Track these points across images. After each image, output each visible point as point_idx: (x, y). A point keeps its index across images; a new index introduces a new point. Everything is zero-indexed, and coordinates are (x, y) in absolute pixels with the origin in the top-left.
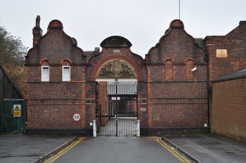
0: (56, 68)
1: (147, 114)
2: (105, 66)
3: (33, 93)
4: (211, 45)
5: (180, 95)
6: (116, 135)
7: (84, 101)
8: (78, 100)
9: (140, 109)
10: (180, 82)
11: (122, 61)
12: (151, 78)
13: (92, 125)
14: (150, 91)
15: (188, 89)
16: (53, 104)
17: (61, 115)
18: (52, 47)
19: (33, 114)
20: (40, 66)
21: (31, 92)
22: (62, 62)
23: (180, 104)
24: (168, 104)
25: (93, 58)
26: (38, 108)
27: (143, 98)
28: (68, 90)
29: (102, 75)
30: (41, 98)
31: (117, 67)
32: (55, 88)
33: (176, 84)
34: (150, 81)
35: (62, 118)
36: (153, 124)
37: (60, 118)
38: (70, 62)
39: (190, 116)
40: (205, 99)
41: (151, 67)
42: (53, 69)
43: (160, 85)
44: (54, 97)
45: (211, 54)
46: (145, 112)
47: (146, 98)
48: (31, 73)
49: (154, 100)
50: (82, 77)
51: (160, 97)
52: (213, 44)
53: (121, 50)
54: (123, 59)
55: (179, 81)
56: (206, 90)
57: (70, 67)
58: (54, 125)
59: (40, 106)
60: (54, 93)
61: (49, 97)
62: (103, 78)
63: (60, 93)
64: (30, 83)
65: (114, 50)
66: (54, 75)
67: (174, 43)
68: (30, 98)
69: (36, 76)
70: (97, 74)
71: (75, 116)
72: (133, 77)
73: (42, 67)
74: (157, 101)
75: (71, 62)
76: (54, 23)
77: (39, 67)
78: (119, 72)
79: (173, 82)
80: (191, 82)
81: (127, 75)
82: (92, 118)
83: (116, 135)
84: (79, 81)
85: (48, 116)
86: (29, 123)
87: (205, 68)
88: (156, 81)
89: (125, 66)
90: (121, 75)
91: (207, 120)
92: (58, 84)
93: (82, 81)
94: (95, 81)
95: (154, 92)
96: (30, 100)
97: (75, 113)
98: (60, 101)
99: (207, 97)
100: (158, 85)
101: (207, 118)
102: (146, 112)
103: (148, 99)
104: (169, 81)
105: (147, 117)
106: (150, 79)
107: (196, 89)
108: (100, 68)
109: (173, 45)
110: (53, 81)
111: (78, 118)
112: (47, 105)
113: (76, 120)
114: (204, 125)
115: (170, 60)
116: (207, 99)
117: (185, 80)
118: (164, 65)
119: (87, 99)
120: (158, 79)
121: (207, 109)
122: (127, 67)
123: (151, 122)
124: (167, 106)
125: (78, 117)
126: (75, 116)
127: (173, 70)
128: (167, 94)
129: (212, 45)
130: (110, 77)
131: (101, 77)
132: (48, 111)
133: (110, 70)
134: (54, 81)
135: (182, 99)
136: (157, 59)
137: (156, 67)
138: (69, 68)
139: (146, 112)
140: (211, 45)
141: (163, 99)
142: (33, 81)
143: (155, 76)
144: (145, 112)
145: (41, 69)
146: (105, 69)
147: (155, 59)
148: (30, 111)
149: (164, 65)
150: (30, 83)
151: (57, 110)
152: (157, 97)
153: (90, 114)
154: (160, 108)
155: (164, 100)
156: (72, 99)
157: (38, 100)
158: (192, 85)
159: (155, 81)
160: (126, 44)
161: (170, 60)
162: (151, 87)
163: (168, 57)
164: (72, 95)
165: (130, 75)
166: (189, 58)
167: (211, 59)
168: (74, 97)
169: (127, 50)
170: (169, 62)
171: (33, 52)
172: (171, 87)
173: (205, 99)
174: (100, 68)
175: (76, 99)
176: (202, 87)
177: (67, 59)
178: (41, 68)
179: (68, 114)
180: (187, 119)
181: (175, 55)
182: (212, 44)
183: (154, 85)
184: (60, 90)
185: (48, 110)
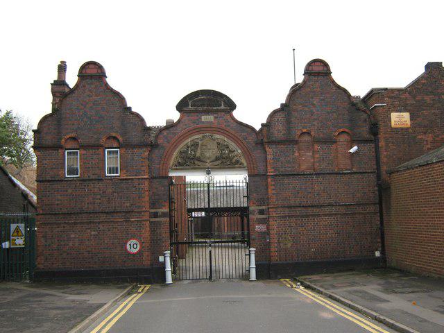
11: (218, 136)
22: (103, 141)
23: (331, 215)
24: (307, 216)
30: (65, 211)
34: (272, 174)
40: (375, 204)
44: (88, 208)
48: (44, 162)
50: (143, 169)
59: (62, 225)
65: (203, 117)
70: (171, 163)
71: (130, 245)
72: (240, 167)
78: (214, 158)
79: (316, 174)
84: (136, 175)
88: (284, 173)
90: (218, 162)
91: (380, 245)
92: (96, 182)
97: (131, 239)
99: (377, 201)
100: (286, 180)
101: (379, 240)
102: (267, 233)
105: (269, 242)
106: (273, 170)
110: (86, 177)
112: (75, 223)
115: (308, 133)
116: (378, 205)
119: (152, 211)
126: (130, 245)
136: (283, 132)
139: (267, 233)
142: (48, 178)
146: (184, 152)
164: (124, 203)
169: (228, 116)
177: (114, 135)
184: (100, 194)
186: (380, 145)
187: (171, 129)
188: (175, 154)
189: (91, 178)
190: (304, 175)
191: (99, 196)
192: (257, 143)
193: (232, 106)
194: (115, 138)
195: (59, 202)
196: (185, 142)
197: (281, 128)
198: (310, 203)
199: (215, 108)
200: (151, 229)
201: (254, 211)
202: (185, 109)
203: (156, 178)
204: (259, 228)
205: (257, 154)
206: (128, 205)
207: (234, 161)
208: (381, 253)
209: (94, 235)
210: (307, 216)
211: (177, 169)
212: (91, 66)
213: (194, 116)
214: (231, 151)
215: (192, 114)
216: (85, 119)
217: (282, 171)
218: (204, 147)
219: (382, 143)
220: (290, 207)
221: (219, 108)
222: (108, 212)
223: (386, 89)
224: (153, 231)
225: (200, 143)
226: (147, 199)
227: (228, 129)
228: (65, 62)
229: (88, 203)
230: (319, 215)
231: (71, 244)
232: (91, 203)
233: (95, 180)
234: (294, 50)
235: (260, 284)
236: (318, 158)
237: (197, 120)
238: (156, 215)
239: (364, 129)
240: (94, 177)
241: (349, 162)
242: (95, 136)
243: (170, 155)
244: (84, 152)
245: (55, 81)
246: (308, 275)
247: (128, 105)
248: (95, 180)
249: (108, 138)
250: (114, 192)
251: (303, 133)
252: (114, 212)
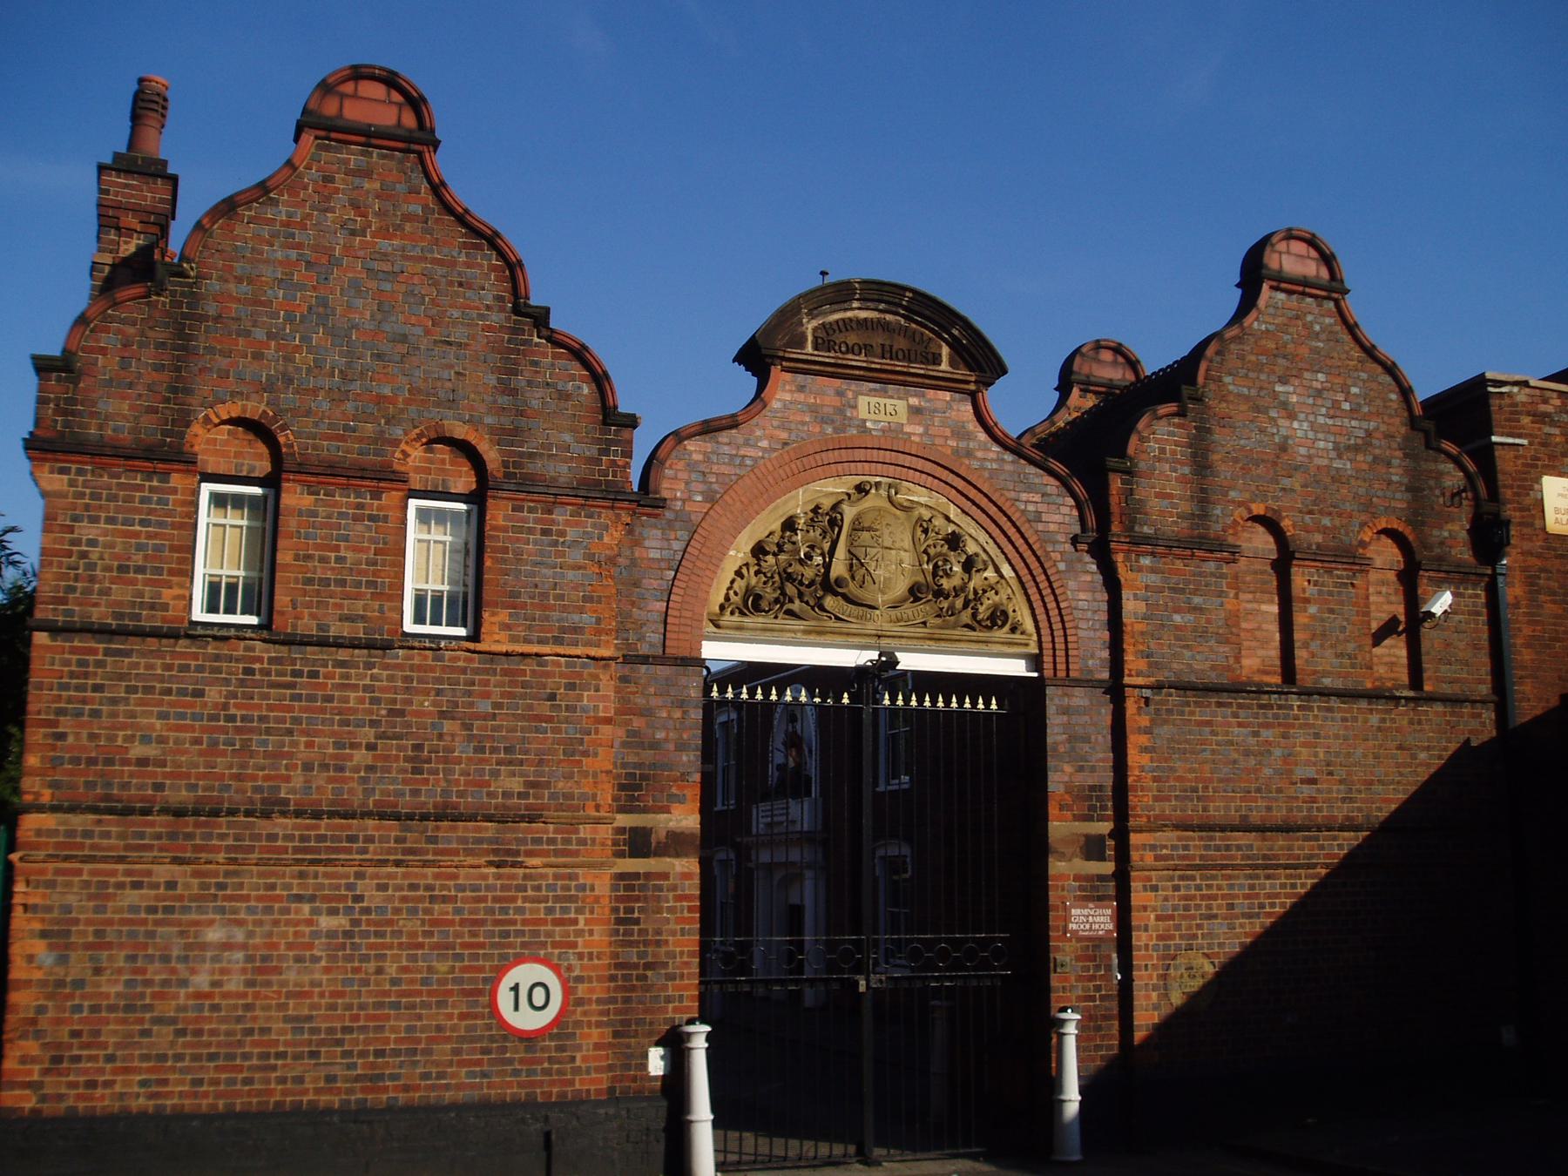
4: (1510, 440)
5: (1344, 800)
9: (1066, 919)
11: (921, 496)
17: (380, 971)
18: (324, 303)
19: (79, 965)
25: (691, 445)
26: (132, 897)
29: (752, 603)
30: (180, 795)
42: (314, 514)
48: (86, 531)
51: (1217, 810)
52: (1520, 436)
53: (914, 401)
60: (309, 745)
63: (371, 747)
65: (863, 401)
68: (54, 785)
69: (140, 570)
71: (516, 988)
75: (490, 466)
76: (355, 96)
77: (176, 480)
82: (669, 1000)
84: (558, 641)
85: (234, 984)
93: (588, 644)
94: (694, 654)
96: (54, 809)
97: (520, 960)
111: (539, 1001)
113: (527, 1020)
119: (623, 820)
125: (539, 996)
129: (1517, 441)
131: (749, 621)
140: (1510, 440)
142: (99, 614)
144: (1100, 939)
148: (44, 934)
151: (340, 922)
152: (1192, 811)
153: (648, 966)
164: (495, 774)
168: (506, 795)
177: (460, 431)
179: (442, 967)
184: (373, 723)
185: (240, 923)
187: (724, 437)
188: (738, 553)
191: (367, 734)
194: (466, 450)
196: (968, 526)
198: (1279, 814)
200: (615, 910)
202: (794, 354)
206: (516, 785)
209: (331, 934)
221: (932, 370)
229: (308, 767)
232: (325, 767)
233: (354, 644)
238: (638, 843)
246: (1050, 1053)
247: (535, 300)
248: (354, 644)
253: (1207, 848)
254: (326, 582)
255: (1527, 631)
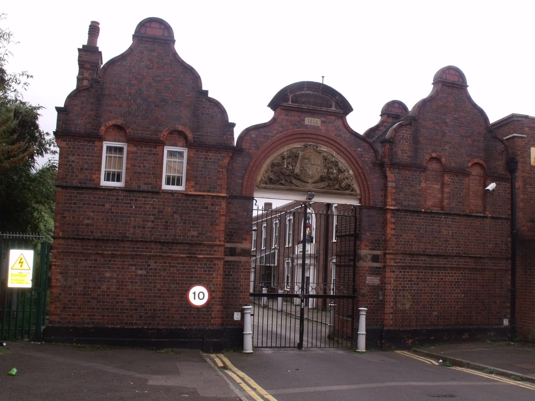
0: (146, 149)
1: (380, 293)
2: (279, 158)
3: (73, 217)
4: (520, 135)
5: (457, 247)
6: (300, 346)
7: (222, 249)
8: (204, 245)
10: (459, 215)
11: (324, 149)
12: (395, 200)
13: (239, 319)
14: (393, 232)
15: (475, 234)
16: (131, 255)
20: (101, 139)
21: (66, 214)
22: (163, 135)
23: (458, 269)
24: (431, 268)
26: (85, 263)
27: (374, 250)
28: (176, 216)
29: (271, 181)
30: (98, 235)
31: (313, 163)
32: (141, 207)
33: (449, 220)
34: (392, 208)
35: (155, 296)
36: (396, 319)
37: (150, 296)
38: (185, 137)
39: (477, 299)
40: (507, 259)
41: (396, 171)
43: (416, 219)
44: (134, 233)
45: (519, 155)
46: (378, 286)
47: (380, 250)
48: (71, 158)
49: (400, 257)
50: (219, 182)
51: (415, 249)
52: (524, 134)
53: (323, 119)
54: (327, 144)
55: (455, 212)
56: (509, 239)
57: (185, 151)
58: (132, 316)
59: (93, 257)
60: (135, 221)
61: (120, 233)
62: (273, 189)
64: (66, 187)
66: (139, 170)
67: (448, 120)
69: (86, 169)
70: (259, 179)
71: (194, 293)
72: (351, 195)
73: (106, 144)
74: (408, 259)
76: (150, 27)
77: (97, 143)
78: (317, 177)
79: (445, 214)
80: (480, 217)
81: (337, 187)
82: (240, 299)
83: (300, 346)
84: (209, 191)
85: (114, 288)
86: (55, 308)
87: (508, 188)
88: (406, 209)
89: (332, 162)
90: (322, 185)
91: (509, 310)
92: (150, 195)
93: (218, 192)
95: (402, 236)
96: (63, 238)
98: (153, 245)
99: (509, 256)
100: (410, 218)
101: (509, 305)
102: (381, 288)
103: (385, 254)
104: (435, 211)
105: (382, 301)
106: (394, 203)
107: (490, 235)
108: (268, 161)
109: (444, 125)
110: (134, 186)
112: (113, 256)
114: (503, 322)
115: (437, 159)
116: (510, 261)
117: (467, 211)
118: (424, 169)
119: (228, 245)
120: (411, 203)
121: (509, 283)
122: (336, 164)
123: (392, 313)
124: (429, 273)
125: (201, 296)
126: (194, 293)
127: (443, 185)
128: (429, 243)
129: (523, 136)
130: (294, 187)
132: (115, 276)
133: (293, 170)
134: (139, 187)
135: (462, 256)
136: (410, 154)
137: (407, 172)
138: (181, 154)
139: (381, 288)
141: (420, 255)
142: (75, 183)
143: (405, 195)
144: (376, 286)
145: (102, 150)
146: (279, 165)
147: (407, 153)
148: (61, 273)
149: (424, 169)
150: (66, 187)
151: (143, 272)
153: (234, 288)
154: (414, 278)
155: (423, 258)
156: (188, 243)
157: (88, 239)
158: (481, 224)
159: (404, 208)
160: (336, 108)
161: (437, 159)
162: (394, 223)
163: (433, 151)
164: (189, 230)
165: (341, 188)
166: (476, 161)
167: (520, 166)
168: (193, 236)
169: (339, 123)
170: (434, 165)
171: (83, 99)
172: (439, 226)
173: (507, 259)
174: (268, 161)
175: (200, 244)
176: (502, 230)
177: (180, 128)
178: (102, 147)
180: (470, 308)
181: (448, 148)
182: (522, 134)
183: (401, 218)
184: (154, 215)
185: (115, 272)
186: (517, 186)
189: (142, 189)
190: (431, 213)
191: (152, 218)
192: (374, 164)
193: (346, 108)
195: (90, 222)
197: (406, 148)
199: (324, 109)
200: (224, 272)
201: (366, 256)
202: (285, 104)
203: (235, 197)
204: (372, 280)
205: (374, 179)
206: (195, 233)
207: (343, 184)
208: (509, 322)
210: (431, 268)
211: (265, 188)
212: (153, 25)
213: (294, 117)
214: (340, 171)
215: (293, 113)
216: (139, 101)
217: (405, 206)
218: (306, 161)
219: (519, 184)
220: (412, 255)
221: (330, 110)
222: (164, 242)
223: (526, 117)
224: (227, 275)
225: (301, 154)
226: (222, 227)
227: (338, 140)
228: (98, 24)
229: (134, 227)
230: (445, 268)
231: (104, 287)
232: (139, 227)
234: (323, 77)
235: (377, 357)
236: (448, 193)
237: (299, 122)
239: (500, 163)
240: (144, 187)
241: (480, 202)
242: (153, 127)
243: (259, 167)
244: (134, 149)
245: (84, 46)
248: (148, 192)
249: (171, 133)
250: (175, 213)
251: (432, 158)
252: (172, 243)
253: (411, 260)
254: (140, 173)
255: (522, 196)
